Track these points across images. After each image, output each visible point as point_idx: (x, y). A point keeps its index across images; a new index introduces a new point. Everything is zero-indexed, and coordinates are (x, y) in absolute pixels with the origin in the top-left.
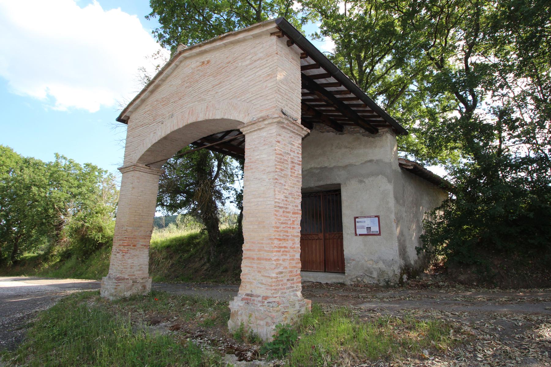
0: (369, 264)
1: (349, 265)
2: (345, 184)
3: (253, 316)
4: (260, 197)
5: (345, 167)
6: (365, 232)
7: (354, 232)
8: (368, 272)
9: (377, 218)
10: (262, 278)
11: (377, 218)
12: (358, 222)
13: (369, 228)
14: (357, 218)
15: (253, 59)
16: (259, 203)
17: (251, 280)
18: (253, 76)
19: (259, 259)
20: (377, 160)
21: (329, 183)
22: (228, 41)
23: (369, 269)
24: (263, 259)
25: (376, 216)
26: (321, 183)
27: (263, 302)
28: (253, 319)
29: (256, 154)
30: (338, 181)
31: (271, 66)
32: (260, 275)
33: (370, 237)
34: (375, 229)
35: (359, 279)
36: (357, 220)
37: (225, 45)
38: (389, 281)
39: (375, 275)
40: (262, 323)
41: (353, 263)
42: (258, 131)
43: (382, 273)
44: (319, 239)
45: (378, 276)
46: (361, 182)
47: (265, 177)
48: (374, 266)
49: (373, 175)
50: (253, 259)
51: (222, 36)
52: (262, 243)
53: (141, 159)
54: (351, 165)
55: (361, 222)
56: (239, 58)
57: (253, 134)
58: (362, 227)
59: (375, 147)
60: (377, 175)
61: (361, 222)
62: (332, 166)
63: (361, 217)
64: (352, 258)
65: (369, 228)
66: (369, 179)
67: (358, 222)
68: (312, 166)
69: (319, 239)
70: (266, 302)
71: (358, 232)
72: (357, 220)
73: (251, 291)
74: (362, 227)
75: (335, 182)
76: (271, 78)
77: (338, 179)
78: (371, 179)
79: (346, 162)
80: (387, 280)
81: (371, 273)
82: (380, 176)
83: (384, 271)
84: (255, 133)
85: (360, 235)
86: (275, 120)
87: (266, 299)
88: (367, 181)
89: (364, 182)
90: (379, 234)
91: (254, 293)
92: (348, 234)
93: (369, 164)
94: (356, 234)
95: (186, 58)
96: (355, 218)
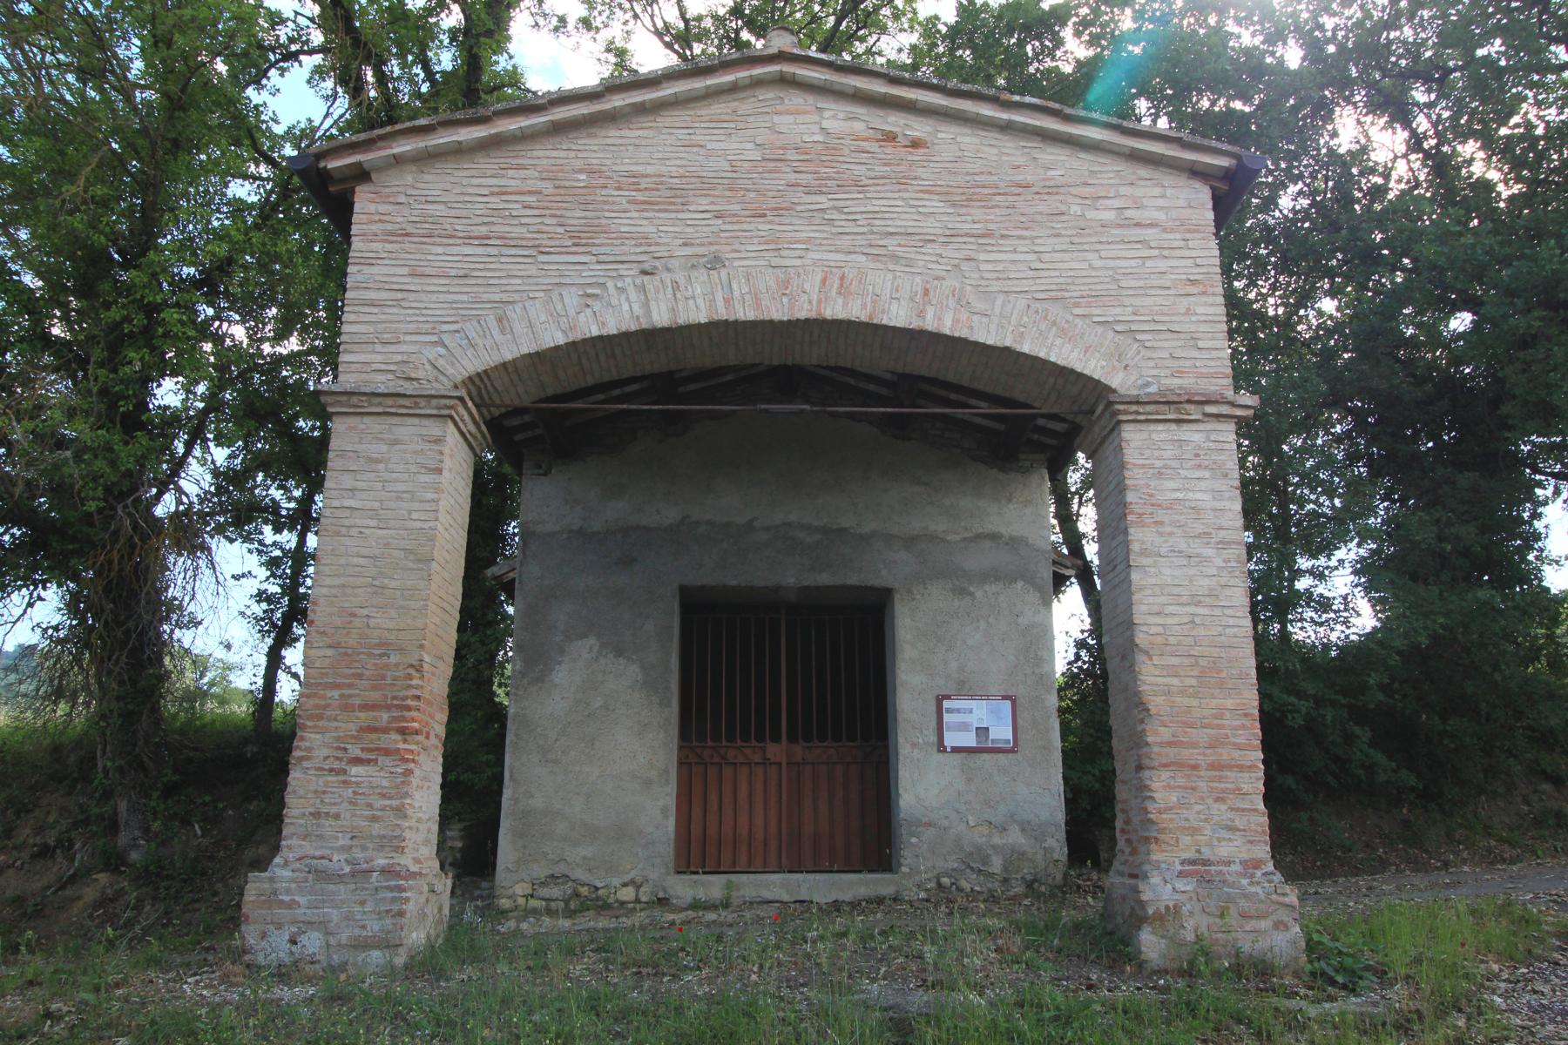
0: (979, 836)
1: (914, 840)
2: (909, 591)
3: (1233, 911)
4: (1198, 604)
5: (910, 541)
6: (970, 740)
7: (934, 739)
8: (975, 860)
9: (1008, 703)
10: (1230, 815)
11: (1008, 703)
12: (949, 711)
13: (982, 732)
14: (948, 697)
15: (1128, 213)
16: (1197, 620)
17: (1195, 824)
18: (1133, 263)
19: (1216, 766)
20: (1012, 538)
21: (853, 580)
22: (1038, 123)
23: (979, 848)
24: (1230, 767)
25: (1005, 698)
26: (825, 579)
27: (1252, 876)
28: (1232, 919)
29: (1171, 485)
30: (883, 579)
31: (1199, 261)
32: (1223, 807)
33: (986, 756)
34: (1002, 732)
35: (946, 881)
36: (946, 704)
37: (1007, 128)
38: (1035, 880)
39: (996, 865)
40: (1263, 924)
41: (930, 833)
42: (1173, 426)
43: (1014, 857)
44: (766, 762)
45: (1006, 869)
46: (962, 592)
47: (1209, 552)
48: (996, 840)
49: (997, 579)
50: (1195, 767)
51: (1017, 98)
52: (1220, 727)
53: (479, 386)
54: (933, 538)
55: (958, 711)
56: (1074, 191)
57: (1152, 427)
58: (964, 727)
59: (1010, 500)
60: (1011, 578)
61: (958, 711)
62: (866, 529)
63: (960, 695)
64: (925, 820)
65: (982, 732)
66: (987, 587)
67: (949, 711)
68: (793, 518)
69: (766, 762)
70: (1259, 873)
71: (951, 740)
72: (946, 704)
73: (1198, 851)
74: (964, 727)
75: (877, 583)
76: (1204, 293)
77: (884, 572)
78: (992, 588)
79: (916, 524)
80: (1029, 877)
81: (986, 860)
82: (1020, 584)
83: (1023, 854)
84: (1160, 427)
85: (956, 750)
86: (1239, 412)
87: (1257, 867)
88: (979, 594)
89: (972, 594)
90: (1012, 751)
91: (1207, 853)
92: (914, 745)
93: (987, 544)
94: (941, 747)
95: (786, 81)
96: (939, 701)
